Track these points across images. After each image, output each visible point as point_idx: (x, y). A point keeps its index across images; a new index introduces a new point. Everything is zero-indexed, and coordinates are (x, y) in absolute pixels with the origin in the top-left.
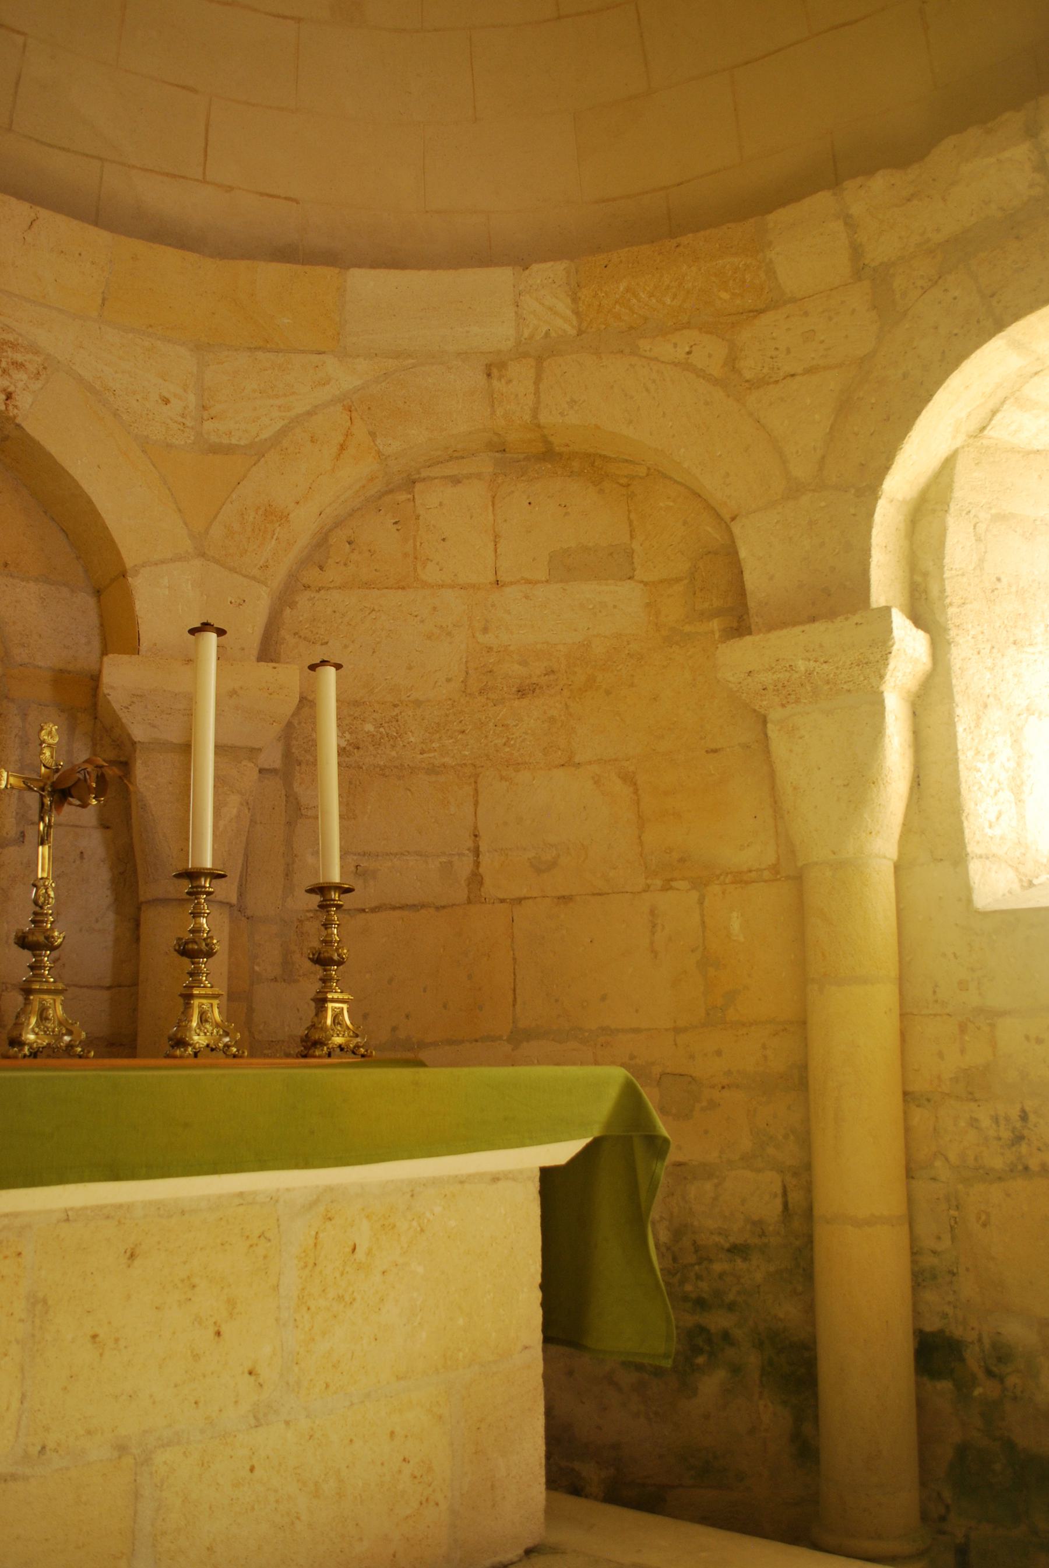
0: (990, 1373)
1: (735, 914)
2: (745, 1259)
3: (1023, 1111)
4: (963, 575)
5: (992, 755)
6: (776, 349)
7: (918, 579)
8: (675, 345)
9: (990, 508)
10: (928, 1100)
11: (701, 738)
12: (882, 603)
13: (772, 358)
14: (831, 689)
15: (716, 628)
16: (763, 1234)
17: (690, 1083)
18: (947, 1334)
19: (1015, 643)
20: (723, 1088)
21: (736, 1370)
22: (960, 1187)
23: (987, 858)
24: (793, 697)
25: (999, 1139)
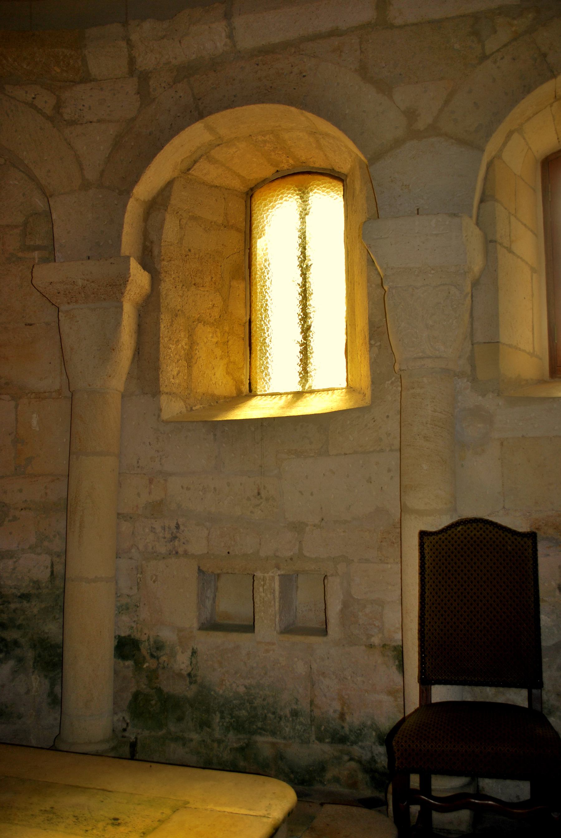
0: (152, 656)
1: (35, 415)
2: (28, 601)
3: (177, 524)
4: (171, 245)
5: (178, 341)
6: (83, 106)
7: (148, 244)
8: (26, 92)
9: (189, 212)
10: (131, 518)
11: (23, 317)
12: (127, 254)
13: (80, 110)
14: (95, 297)
15: (36, 257)
16: (39, 588)
17: (3, 506)
18: (132, 637)
19: (195, 284)
20: (22, 509)
21: (20, 660)
22: (144, 562)
23: (170, 394)
24: (74, 299)
25: (165, 538)
